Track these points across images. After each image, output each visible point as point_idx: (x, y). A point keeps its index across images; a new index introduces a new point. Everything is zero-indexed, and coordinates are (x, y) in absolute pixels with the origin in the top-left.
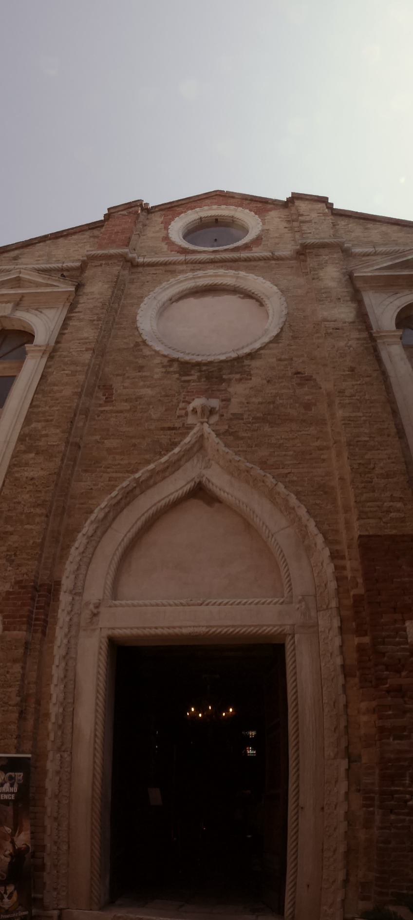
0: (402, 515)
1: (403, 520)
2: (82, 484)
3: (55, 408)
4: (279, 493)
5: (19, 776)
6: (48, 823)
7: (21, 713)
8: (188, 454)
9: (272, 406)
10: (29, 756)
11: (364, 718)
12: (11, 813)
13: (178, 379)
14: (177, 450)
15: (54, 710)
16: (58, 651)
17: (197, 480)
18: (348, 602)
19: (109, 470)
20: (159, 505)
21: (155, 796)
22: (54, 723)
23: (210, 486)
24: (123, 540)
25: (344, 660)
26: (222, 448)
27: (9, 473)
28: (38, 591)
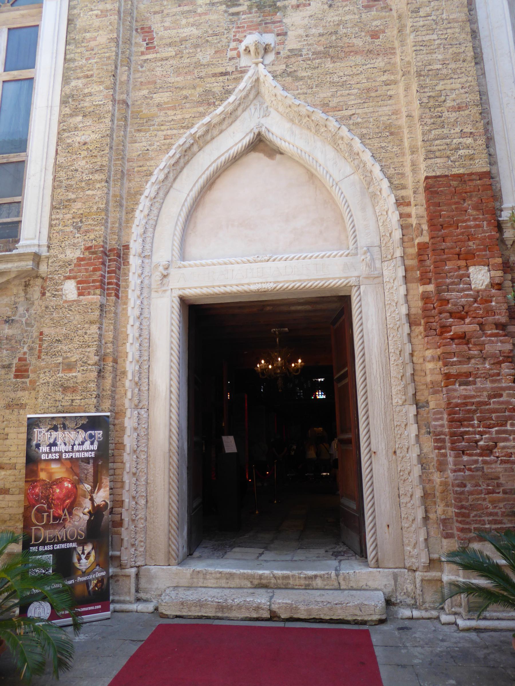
0: (471, 152)
1: (471, 158)
2: (137, 145)
4: (342, 138)
5: (99, 434)
6: (126, 478)
7: (100, 372)
8: (243, 104)
9: (334, 38)
10: (108, 414)
11: (430, 366)
13: (226, 12)
14: (231, 99)
15: (130, 367)
16: (132, 310)
17: (256, 132)
18: (414, 251)
19: (162, 128)
20: (219, 162)
21: (230, 445)
22: (131, 380)
23: (270, 136)
24: (186, 200)
25: (409, 308)
26: (280, 91)
27: (60, 140)
28: (108, 256)
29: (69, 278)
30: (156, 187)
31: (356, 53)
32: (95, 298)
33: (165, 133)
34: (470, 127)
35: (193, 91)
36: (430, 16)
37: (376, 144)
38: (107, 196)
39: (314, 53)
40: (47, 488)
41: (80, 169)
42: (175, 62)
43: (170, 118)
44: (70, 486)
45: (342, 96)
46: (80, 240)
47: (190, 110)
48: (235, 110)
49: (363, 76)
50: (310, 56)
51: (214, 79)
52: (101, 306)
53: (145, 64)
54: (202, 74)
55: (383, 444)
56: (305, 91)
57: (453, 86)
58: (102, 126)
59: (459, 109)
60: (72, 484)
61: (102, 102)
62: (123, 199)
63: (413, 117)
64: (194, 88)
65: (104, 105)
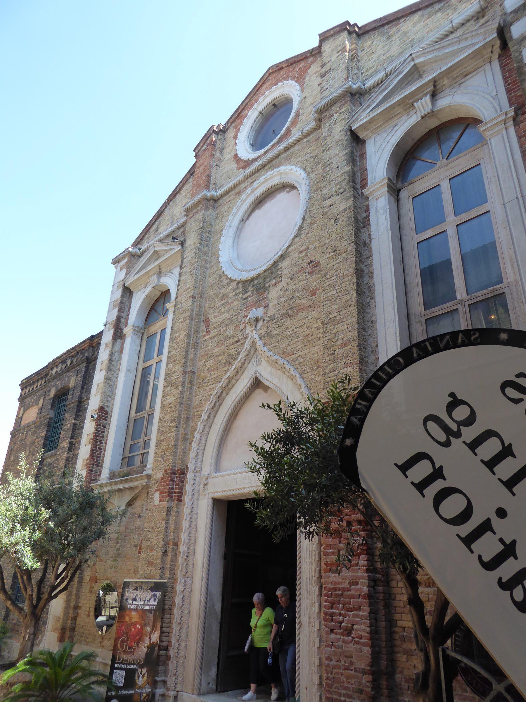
5: (159, 594)
10: (165, 581)
12: (152, 618)
13: (242, 298)
15: (182, 548)
16: (186, 511)
17: (254, 377)
30: (203, 425)
31: (303, 309)
33: (209, 388)
34: (350, 358)
39: (281, 316)
45: (293, 344)
55: (307, 617)
64: (224, 354)
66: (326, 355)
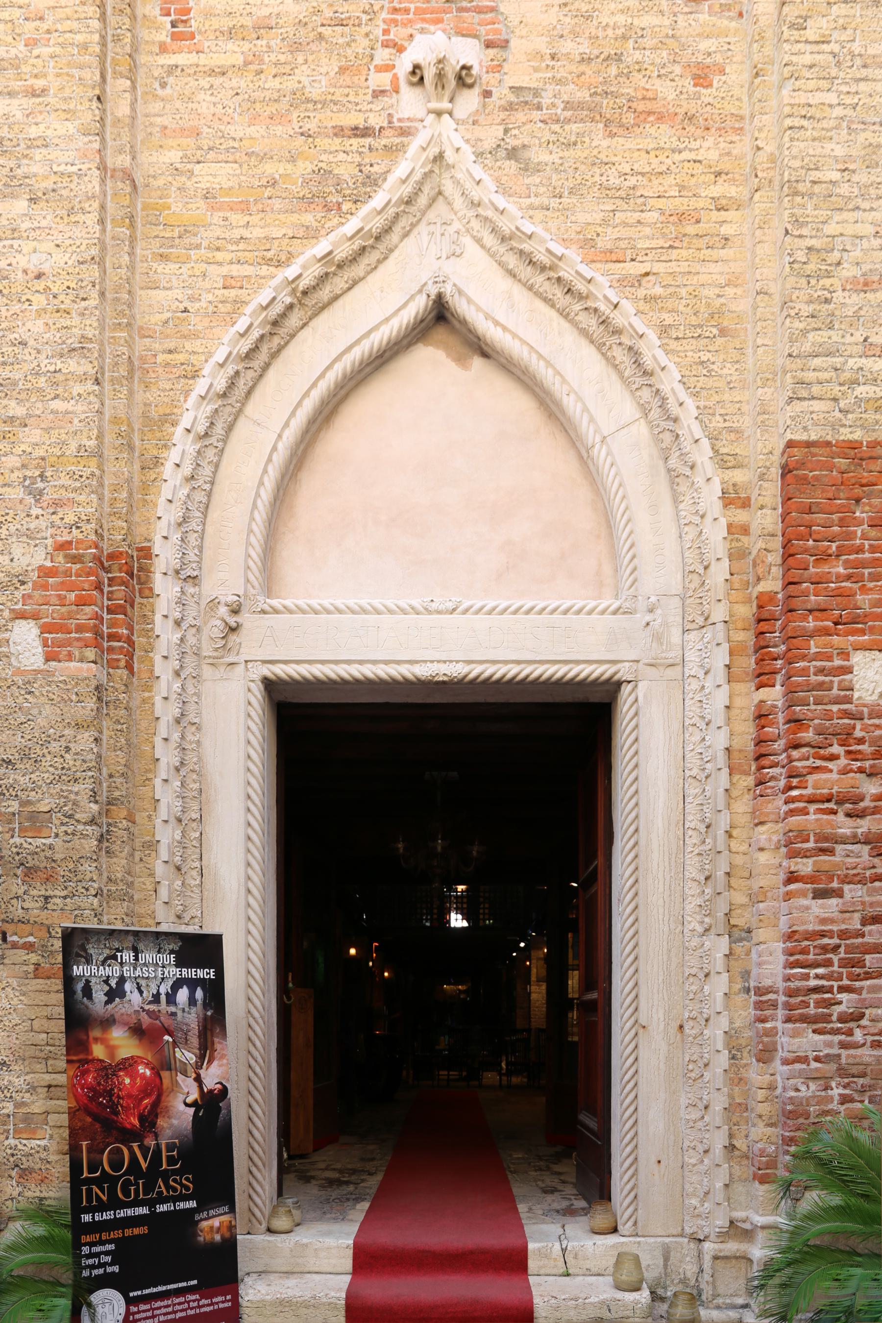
3: (46, 51)
9: (613, 70)
14: (378, 200)
17: (433, 291)
19: (220, 256)
24: (274, 449)
29: (21, 616)
31: (661, 118)
32: (82, 668)
33: (225, 270)
35: (289, 166)
36: (828, 42)
37: (690, 354)
38: (100, 420)
39: (568, 106)
40: (107, 1075)
41: (31, 343)
42: (243, 84)
43: (237, 233)
44: (148, 1072)
45: (626, 224)
46: (42, 523)
47: (282, 217)
48: (388, 230)
49: (670, 180)
50: (559, 111)
51: (338, 141)
52: (97, 688)
53: (171, 80)
54: (311, 126)
56: (546, 201)
57: (861, 229)
58: (78, 232)
59: (866, 286)
60: (152, 1069)
61: (74, 169)
62: (133, 430)
63: (770, 295)
64: (293, 160)
65: (79, 176)
66: (803, 295)
